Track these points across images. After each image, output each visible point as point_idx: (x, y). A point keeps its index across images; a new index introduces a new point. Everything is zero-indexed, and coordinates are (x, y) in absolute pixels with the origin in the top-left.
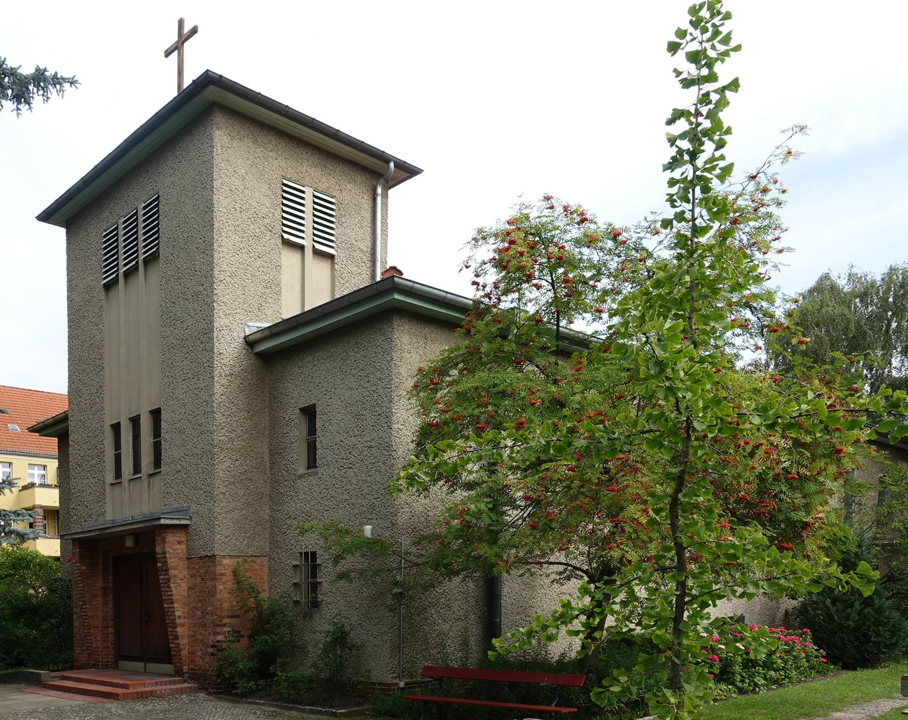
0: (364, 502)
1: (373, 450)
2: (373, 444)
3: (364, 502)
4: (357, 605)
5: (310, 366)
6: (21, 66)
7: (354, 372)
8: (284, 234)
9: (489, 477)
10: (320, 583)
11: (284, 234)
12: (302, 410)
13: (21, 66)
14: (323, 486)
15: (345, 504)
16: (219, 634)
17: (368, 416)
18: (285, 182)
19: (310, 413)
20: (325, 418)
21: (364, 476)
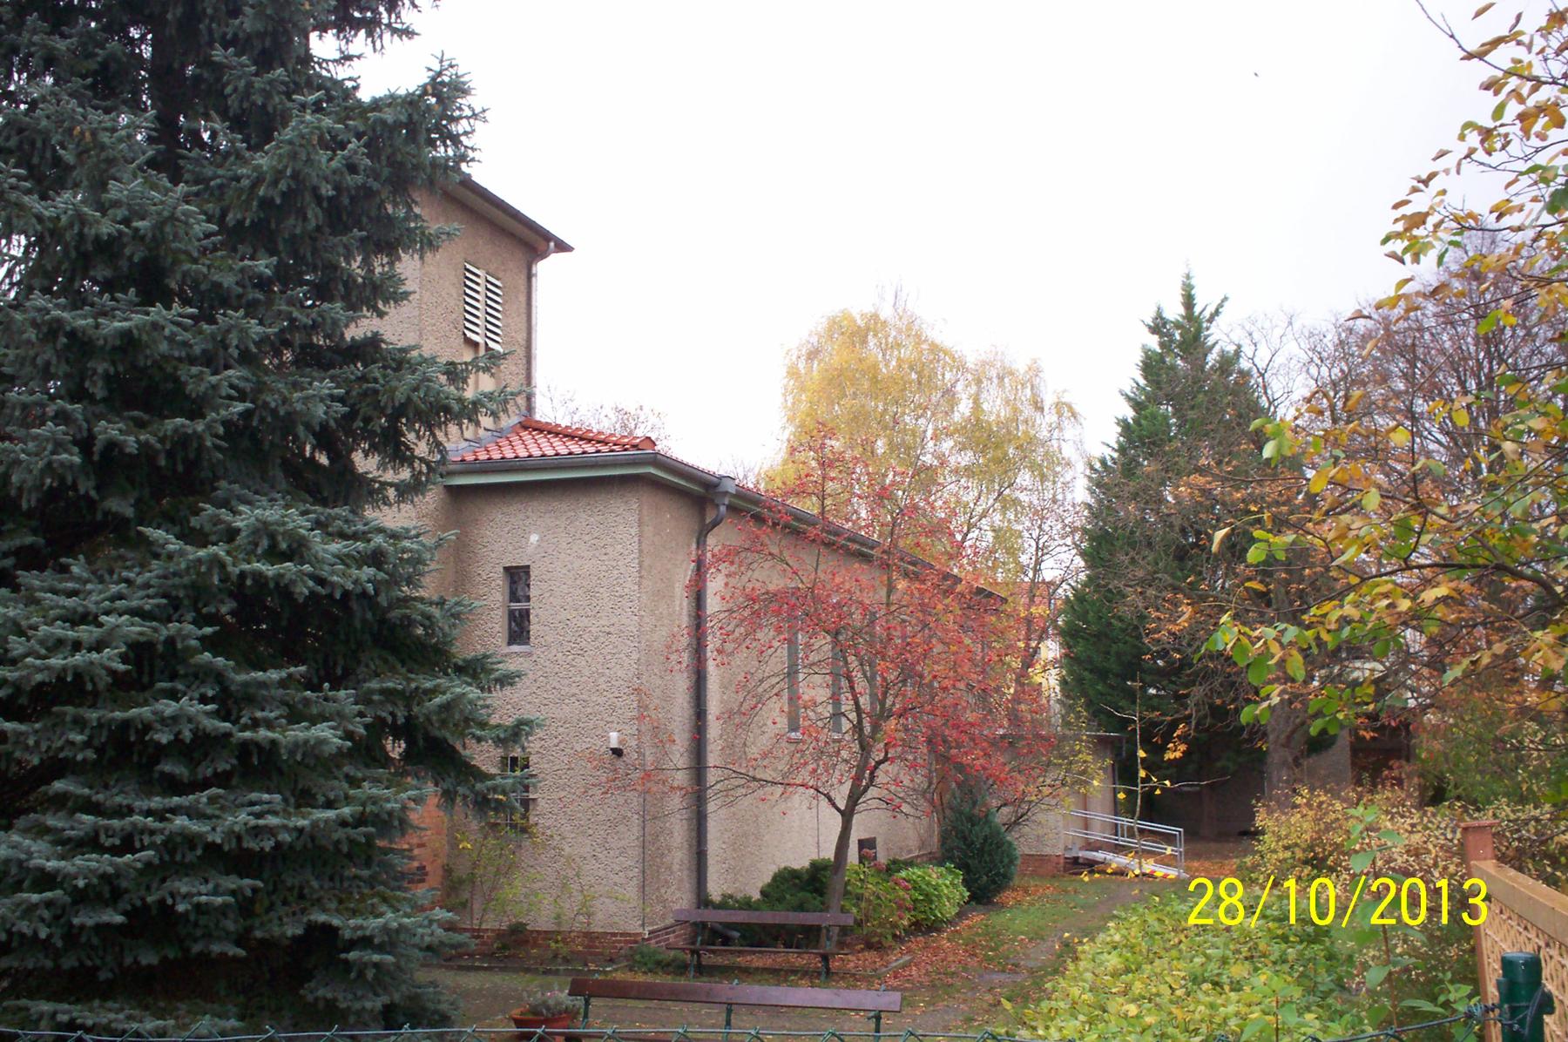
0: (601, 700)
1: (613, 638)
2: (612, 629)
3: (601, 700)
4: (590, 832)
5: (521, 516)
6: (1225, 299)
7: (586, 538)
8: (466, 332)
9: (1182, 570)
10: (534, 800)
11: (466, 332)
12: (507, 569)
13: (1225, 299)
14: (541, 673)
15: (573, 699)
16: (91, 959)
17: (606, 595)
18: (468, 266)
19: (517, 577)
20: (544, 586)
21: (599, 666)
